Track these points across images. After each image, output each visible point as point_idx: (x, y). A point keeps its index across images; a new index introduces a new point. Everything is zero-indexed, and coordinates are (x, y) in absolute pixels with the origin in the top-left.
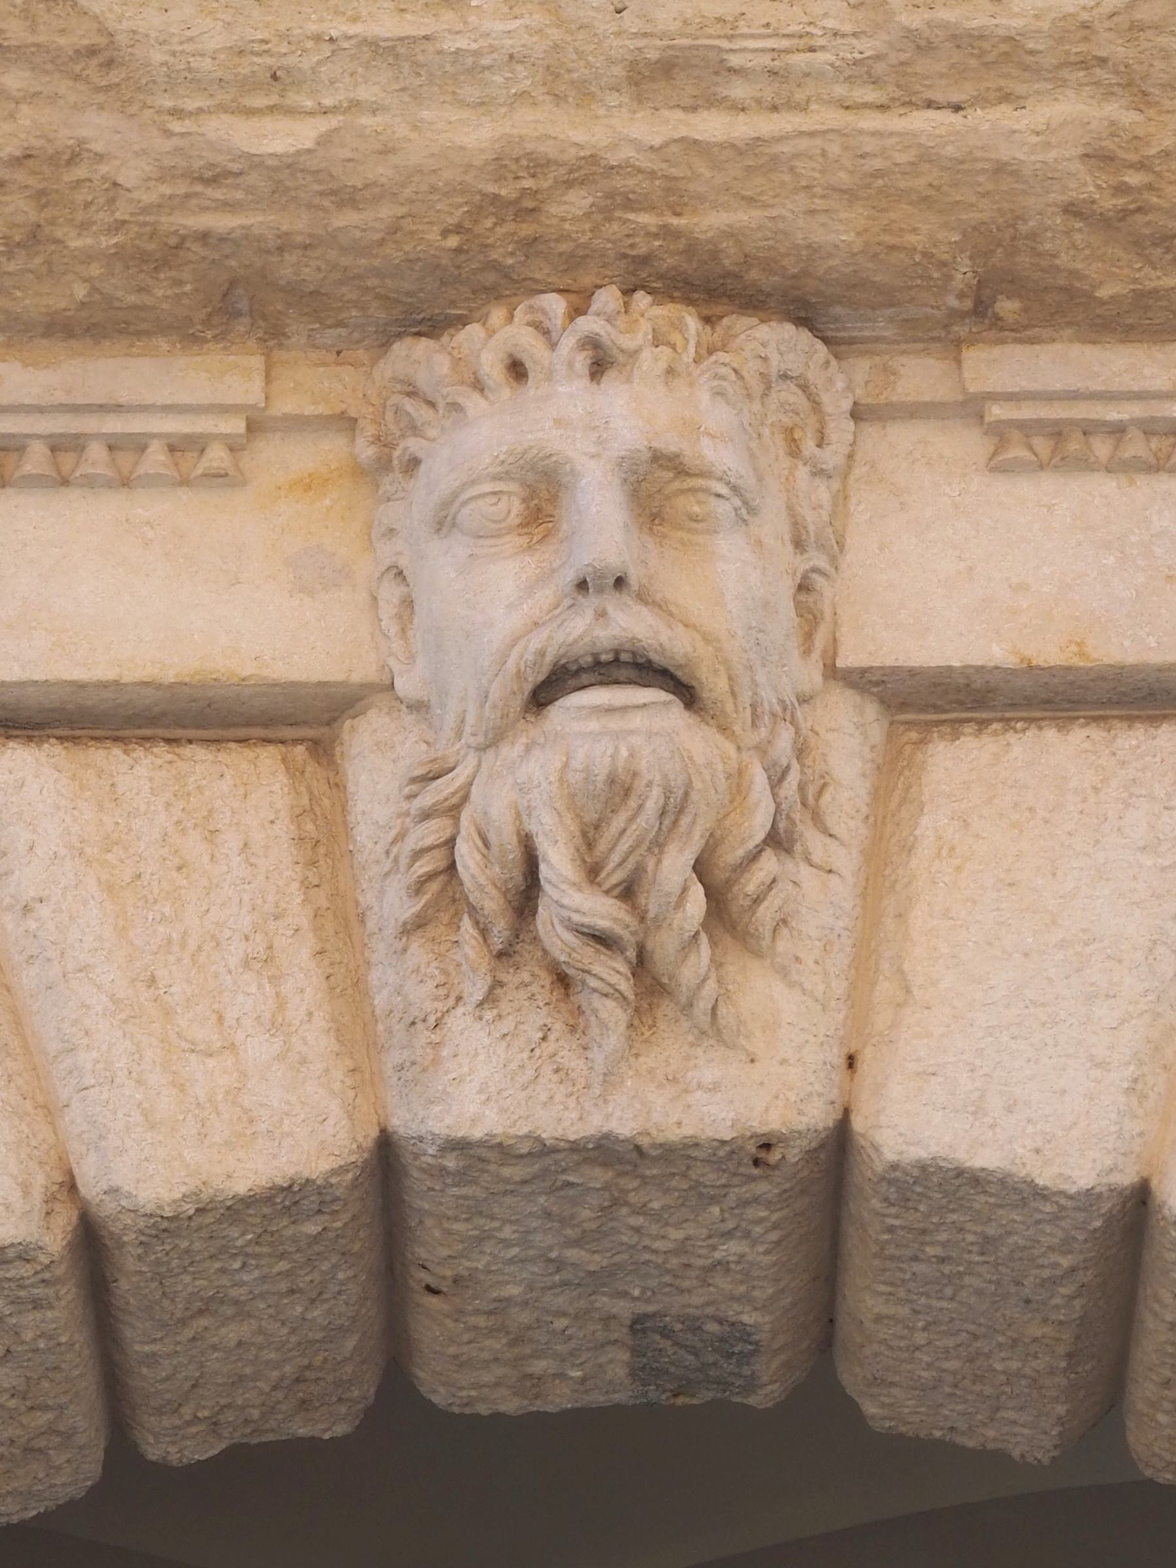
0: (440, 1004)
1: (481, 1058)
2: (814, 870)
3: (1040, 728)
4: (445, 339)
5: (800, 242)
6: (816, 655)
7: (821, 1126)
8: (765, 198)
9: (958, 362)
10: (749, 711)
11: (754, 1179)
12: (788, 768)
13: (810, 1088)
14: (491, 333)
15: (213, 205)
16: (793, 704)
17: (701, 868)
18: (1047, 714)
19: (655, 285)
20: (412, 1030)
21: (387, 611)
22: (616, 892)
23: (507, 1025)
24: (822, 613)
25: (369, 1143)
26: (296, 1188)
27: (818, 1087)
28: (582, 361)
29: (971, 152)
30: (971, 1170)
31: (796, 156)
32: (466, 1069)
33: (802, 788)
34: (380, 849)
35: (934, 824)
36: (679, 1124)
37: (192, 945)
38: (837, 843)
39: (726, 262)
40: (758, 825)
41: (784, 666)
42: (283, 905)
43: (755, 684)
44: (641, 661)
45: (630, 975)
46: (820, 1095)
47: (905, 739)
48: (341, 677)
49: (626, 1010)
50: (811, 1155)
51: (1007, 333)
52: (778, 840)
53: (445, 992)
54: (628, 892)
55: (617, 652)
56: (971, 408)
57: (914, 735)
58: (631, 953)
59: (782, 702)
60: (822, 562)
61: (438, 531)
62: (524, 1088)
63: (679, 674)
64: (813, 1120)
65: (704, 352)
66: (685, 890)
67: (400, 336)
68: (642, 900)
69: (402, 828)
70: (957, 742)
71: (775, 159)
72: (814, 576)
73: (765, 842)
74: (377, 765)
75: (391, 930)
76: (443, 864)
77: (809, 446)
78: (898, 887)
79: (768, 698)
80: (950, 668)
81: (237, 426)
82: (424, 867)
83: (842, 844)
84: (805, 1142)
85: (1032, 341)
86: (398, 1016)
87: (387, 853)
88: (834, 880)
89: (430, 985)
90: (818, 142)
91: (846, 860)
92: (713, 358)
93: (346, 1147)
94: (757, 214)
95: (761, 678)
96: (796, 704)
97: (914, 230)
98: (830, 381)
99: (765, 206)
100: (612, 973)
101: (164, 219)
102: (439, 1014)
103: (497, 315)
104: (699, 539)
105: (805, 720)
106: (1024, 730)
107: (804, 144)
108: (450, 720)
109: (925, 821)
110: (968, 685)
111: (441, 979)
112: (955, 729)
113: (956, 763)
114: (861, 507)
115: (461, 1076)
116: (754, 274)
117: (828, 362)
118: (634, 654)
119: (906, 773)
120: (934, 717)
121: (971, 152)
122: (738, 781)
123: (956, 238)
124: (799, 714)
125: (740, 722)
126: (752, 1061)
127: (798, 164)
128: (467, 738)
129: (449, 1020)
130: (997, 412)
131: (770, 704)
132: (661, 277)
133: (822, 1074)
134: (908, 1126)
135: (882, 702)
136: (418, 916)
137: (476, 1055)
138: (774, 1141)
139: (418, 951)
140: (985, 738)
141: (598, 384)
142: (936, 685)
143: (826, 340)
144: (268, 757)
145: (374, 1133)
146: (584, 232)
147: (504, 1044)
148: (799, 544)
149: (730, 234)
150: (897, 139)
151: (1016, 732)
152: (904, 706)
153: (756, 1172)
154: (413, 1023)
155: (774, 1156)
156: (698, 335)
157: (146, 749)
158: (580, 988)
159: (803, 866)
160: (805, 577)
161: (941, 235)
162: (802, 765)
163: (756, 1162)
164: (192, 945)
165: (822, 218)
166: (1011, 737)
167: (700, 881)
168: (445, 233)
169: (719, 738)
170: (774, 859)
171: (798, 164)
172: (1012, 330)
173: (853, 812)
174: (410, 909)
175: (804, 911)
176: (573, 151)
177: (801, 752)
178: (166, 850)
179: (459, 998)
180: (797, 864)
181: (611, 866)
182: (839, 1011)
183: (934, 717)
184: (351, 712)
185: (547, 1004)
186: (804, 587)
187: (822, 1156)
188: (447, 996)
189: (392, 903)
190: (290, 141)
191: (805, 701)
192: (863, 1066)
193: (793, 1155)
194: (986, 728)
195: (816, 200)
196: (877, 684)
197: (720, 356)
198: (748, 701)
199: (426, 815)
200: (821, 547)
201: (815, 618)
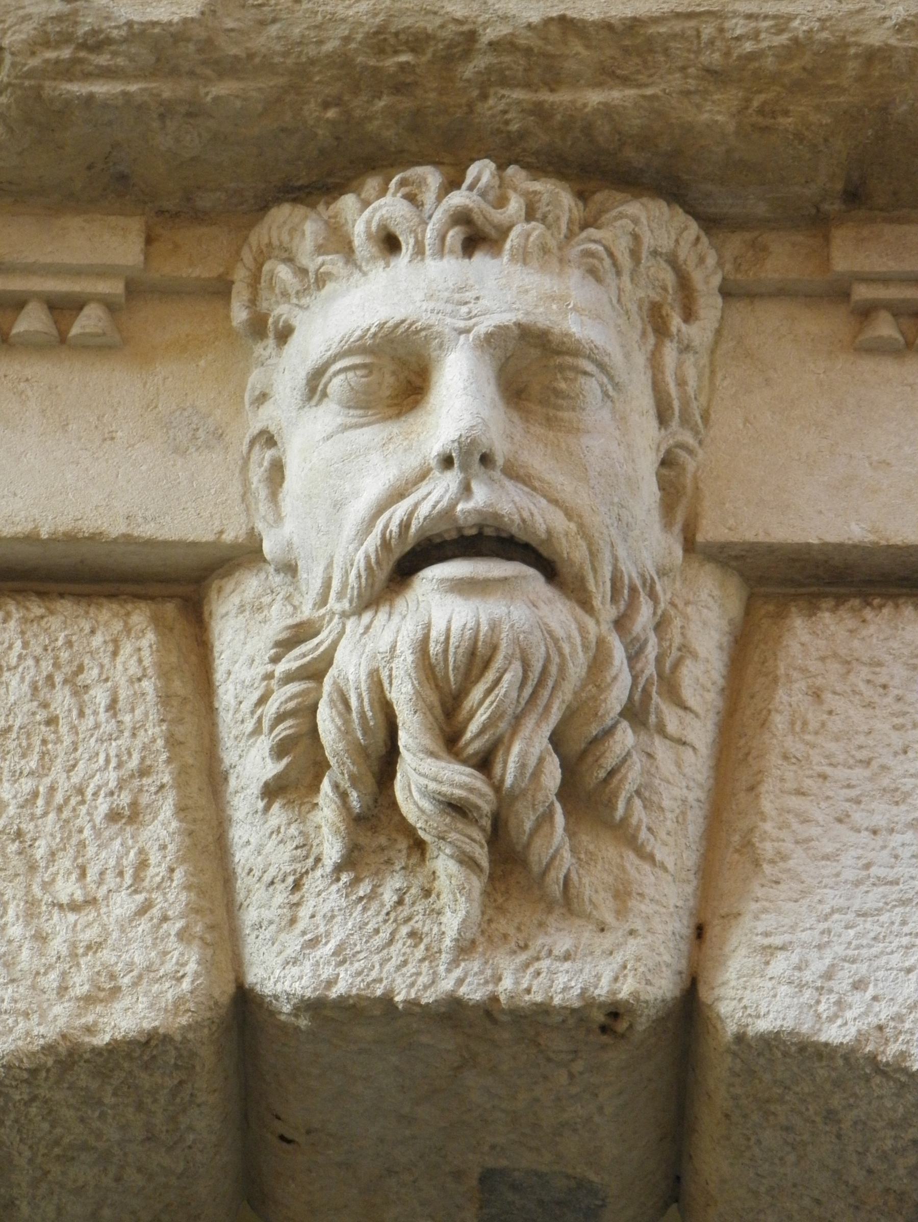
0: (299, 865)
1: (339, 919)
2: (668, 742)
3: (897, 606)
4: (321, 207)
5: (674, 121)
6: (677, 528)
7: (669, 995)
8: (640, 77)
9: (827, 239)
10: (608, 584)
11: (604, 1047)
12: (646, 641)
13: (658, 958)
14: (366, 204)
15: (97, 71)
16: (652, 579)
17: (556, 740)
18: (904, 591)
19: (529, 160)
20: (271, 889)
21: (257, 475)
22: (474, 761)
23: (364, 889)
24: (684, 487)
25: (225, 1000)
26: (153, 1043)
27: (667, 958)
28: (455, 236)
29: (844, 38)
30: (816, 1044)
31: (674, 36)
32: (322, 929)
33: (659, 660)
34: (246, 707)
35: (789, 698)
36: (528, 991)
37: (59, 798)
38: (692, 715)
39: (601, 139)
40: (617, 696)
41: (645, 540)
42: (148, 762)
43: (615, 559)
44: (504, 535)
45: (483, 842)
46: (668, 965)
47: (763, 612)
48: (210, 537)
49: (479, 877)
50: (660, 1021)
51: (877, 212)
52: (636, 713)
53: (304, 853)
54: (484, 763)
55: (481, 527)
56: (837, 293)
57: (771, 608)
58: (486, 823)
59: (642, 576)
60: (688, 438)
61: (310, 398)
62: (379, 950)
63: (541, 550)
64: (661, 992)
65: (576, 228)
66: (541, 760)
67: (278, 201)
68: (497, 770)
69: (267, 690)
70: (814, 619)
71: (650, 40)
72: (679, 451)
73: (621, 714)
74: (243, 640)
75: (255, 788)
76: (305, 728)
77: (676, 322)
78: (750, 759)
79: (629, 571)
80: (809, 545)
81: (114, 288)
82: (284, 729)
83: (697, 716)
84: (652, 1012)
85: (900, 221)
86: (257, 873)
87: (253, 713)
88: (688, 755)
89: (290, 846)
90: (692, 23)
91: (701, 734)
92: (584, 235)
93: (202, 1003)
94: (631, 92)
95: (621, 553)
96: (656, 578)
97: (786, 113)
98: (702, 260)
99: (640, 86)
100: (468, 841)
101: (47, 83)
102: (298, 875)
103: (372, 184)
104: (565, 415)
105: (664, 591)
106: (881, 607)
107: (677, 26)
108: (316, 585)
109: (781, 694)
110: (826, 562)
111: (299, 841)
112: (812, 607)
113: (810, 639)
114: (725, 383)
115: (317, 937)
116: (629, 153)
117: (698, 239)
118: (498, 529)
119: (762, 646)
120: (792, 591)
121: (844, 38)
122: (599, 661)
123: (827, 120)
124: (658, 587)
125: (600, 592)
126: (602, 930)
127: (672, 44)
128: (333, 604)
129: (307, 882)
130: (863, 292)
131: (630, 578)
132: (537, 153)
133: (671, 945)
134: (756, 997)
135: (742, 575)
136: (278, 777)
137: (333, 917)
138: (622, 1011)
139: (278, 815)
140: (843, 612)
141: (470, 257)
142: (794, 560)
143: (697, 217)
144: (140, 617)
145: (231, 989)
146: (460, 106)
147: (360, 907)
148: (663, 418)
149: (608, 111)
150: (771, 23)
151: (873, 608)
152: (762, 580)
153: (605, 1039)
154: (272, 883)
155: (622, 1026)
156: (570, 211)
157: (18, 603)
158: (435, 853)
159: (657, 740)
160: (668, 452)
161: (814, 117)
162: (661, 639)
163: (604, 1029)
164: (59, 798)
165: (697, 99)
166: (868, 613)
167: (556, 750)
168: (326, 105)
169: (578, 611)
170: (629, 731)
171: (672, 44)
172: (882, 210)
173: (709, 685)
174: (272, 769)
175: (657, 781)
176: (452, 27)
177: (661, 626)
178: (35, 704)
179: (318, 860)
180: (651, 736)
181: (468, 735)
182: (689, 882)
183: (792, 591)
184: (220, 571)
185: (403, 868)
186: (667, 462)
187: (670, 1025)
188: (307, 857)
189: (252, 763)
190: (174, 9)
191: (664, 575)
192: (710, 933)
193: (642, 1025)
194: (843, 604)
195: (689, 80)
196: (736, 558)
197: (592, 231)
198: (608, 575)
199: (289, 678)
200: (685, 420)
201: (678, 492)
